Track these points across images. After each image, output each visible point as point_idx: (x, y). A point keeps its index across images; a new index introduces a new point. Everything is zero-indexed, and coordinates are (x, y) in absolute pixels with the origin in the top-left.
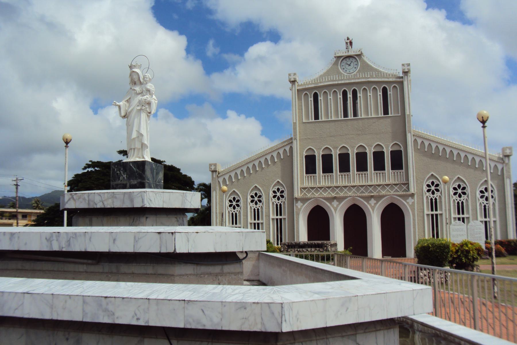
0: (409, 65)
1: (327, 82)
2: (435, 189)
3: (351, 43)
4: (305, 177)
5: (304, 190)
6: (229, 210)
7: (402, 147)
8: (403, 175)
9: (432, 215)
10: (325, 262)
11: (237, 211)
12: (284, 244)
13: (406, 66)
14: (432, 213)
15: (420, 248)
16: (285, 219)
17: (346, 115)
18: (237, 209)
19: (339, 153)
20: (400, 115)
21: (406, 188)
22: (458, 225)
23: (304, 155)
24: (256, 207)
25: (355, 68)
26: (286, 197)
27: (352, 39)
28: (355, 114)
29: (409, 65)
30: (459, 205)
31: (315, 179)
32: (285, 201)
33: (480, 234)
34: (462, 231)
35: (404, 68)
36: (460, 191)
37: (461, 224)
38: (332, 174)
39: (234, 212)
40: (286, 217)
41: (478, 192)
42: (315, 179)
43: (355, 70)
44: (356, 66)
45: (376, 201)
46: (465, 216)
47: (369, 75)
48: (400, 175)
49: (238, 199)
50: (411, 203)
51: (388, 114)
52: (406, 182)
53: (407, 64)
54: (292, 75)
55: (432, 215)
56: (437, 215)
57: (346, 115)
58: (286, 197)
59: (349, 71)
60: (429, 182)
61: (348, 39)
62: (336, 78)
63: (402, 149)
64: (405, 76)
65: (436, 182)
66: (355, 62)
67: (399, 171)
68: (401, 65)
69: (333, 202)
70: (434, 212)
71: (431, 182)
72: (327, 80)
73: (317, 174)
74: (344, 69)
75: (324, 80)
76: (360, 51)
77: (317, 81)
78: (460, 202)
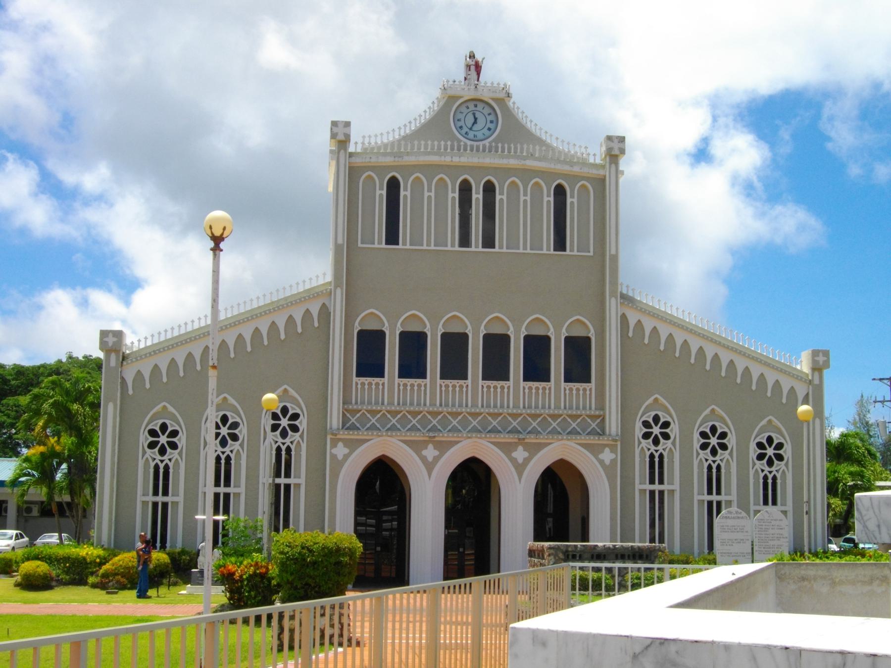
0: (347, 124)
1: (429, 154)
2: (714, 436)
3: (478, 68)
4: (482, 386)
5: (495, 419)
6: (147, 456)
7: (592, 331)
8: (590, 394)
9: (652, 493)
10: (601, 595)
11: (170, 460)
12: (557, 549)
13: (616, 141)
14: (652, 487)
15: (283, 566)
16: (672, 492)
17: (465, 241)
18: (778, 465)
19: (402, 330)
20: (591, 254)
21: (495, 426)
22: (734, 518)
23: (564, 334)
24: (223, 453)
25: (489, 129)
26: (142, 431)
27: (484, 59)
28: (489, 241)
29: (347, 124)
30: (712, 472)
31: (381, 390)
32: (301, 442)
33: (778, 539)
34: (742, 532)
35: (611, 145)
36: (714, 441)
37: (739, 516)
38: (547, 383)
39: (162, 461)
40: (302, 481)
41: (753, 446)
42: (547, 395)
43: (487, 133)
44: (492, 126)
45: (528, 452)
46: (722, 498)
47: (525, 152)
48: (544, 393)
49: (173, 428)
50: (607, 462)
51: (564, 250)
52: (597, 413)
53: (618, 137)
54: (341, 126)
55: (652, 493)
56: (661, 493)
57: (465, 241)
58: (142, 431)
59: (475, 136)
60: (649, 417)
61: (472, 56)
62: (419, 149)
63: (592, 335)
64: (610, 164)
65: (663, 416)
66: (489, 114)
67: (581, 386)
68: (348, 120)
69: (426, 450)
70: (657, 487)
71: (652, 417)
72: (512, 153)
73: (469, 381)
74: (461, 127)
75: (415, 150)
76: (504, 91)
77: (399, 148)
78: (714, 466)
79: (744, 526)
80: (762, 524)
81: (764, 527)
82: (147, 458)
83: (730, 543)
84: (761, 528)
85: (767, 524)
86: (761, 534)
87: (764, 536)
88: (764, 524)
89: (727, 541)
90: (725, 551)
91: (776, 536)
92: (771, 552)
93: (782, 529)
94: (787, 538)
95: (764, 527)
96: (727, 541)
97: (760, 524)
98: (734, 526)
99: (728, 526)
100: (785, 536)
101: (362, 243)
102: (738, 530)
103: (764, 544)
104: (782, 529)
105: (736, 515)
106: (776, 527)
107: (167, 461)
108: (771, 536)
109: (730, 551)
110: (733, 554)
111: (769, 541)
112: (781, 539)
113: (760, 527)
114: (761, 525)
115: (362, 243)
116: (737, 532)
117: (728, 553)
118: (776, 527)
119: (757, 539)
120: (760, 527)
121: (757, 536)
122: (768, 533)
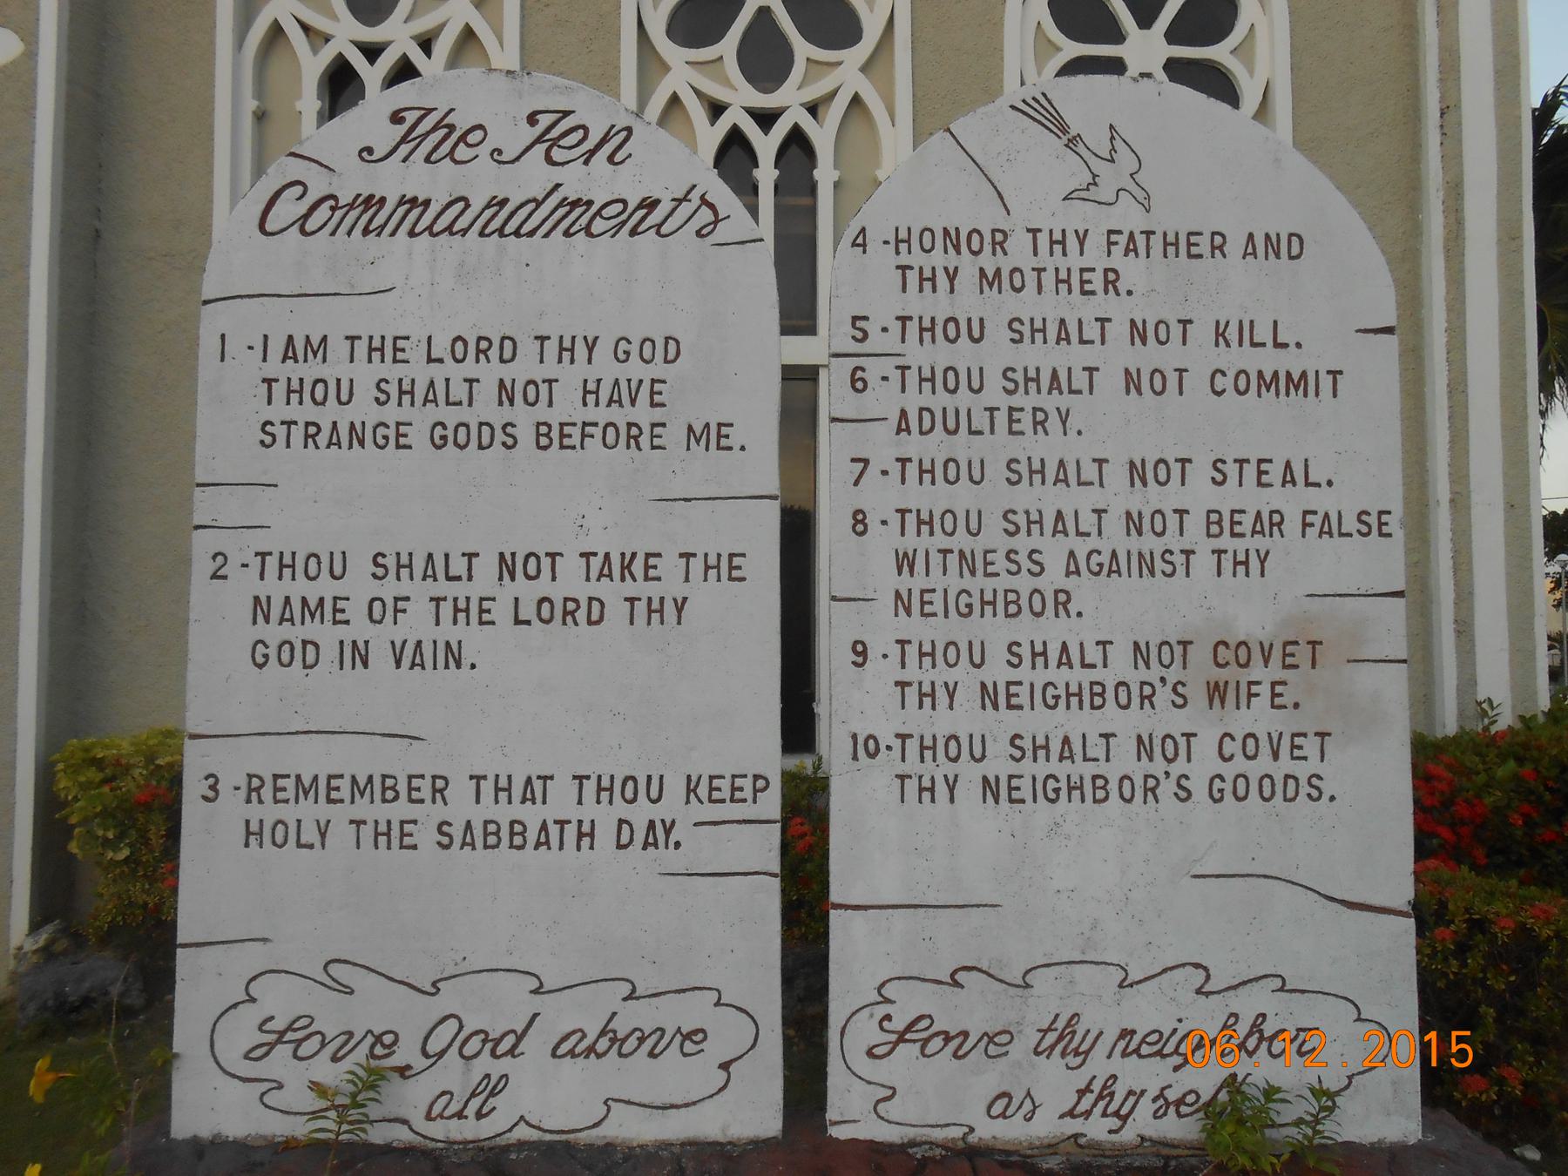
79: (672, 348)
80: (968, 302)
81: (997, 353)
82: (675, 100)
83: (417, 624)
84: (950, 378)
85: (1048, 306)
86: (951, 471)
87: (995, 496)
88: (999, 307)
89: (359, 586)
90: (311, 759)
91: (1199, 494)
92: (1125, 760)
93: (1297, 383)
94: (1372, 524)
95: (997, 353)
96: (359, 586)
97: (920, 304)
98: (508, 348)
99: (389, 348)
100: (1342, 501)
101: (1457, 1037)
102: (567, 406)
103: (995, 632)
104: (1297, 383)
105: (532, 177)
106: (1201, 355)
107: (796, 116)
108: (1119, 496)
109: (397, 761)
110: (461, 807)
111: (1084, 590)
112: (1288, 547)
113: (938, 355)
114: (951, 329)
115: (1457, 1037)
116: (544, 436)
117: (388, 789)
118: (1201, 355)
119: (883, 542)
120: (938, 355)
121: (881, 497)
122: (1048, 447)
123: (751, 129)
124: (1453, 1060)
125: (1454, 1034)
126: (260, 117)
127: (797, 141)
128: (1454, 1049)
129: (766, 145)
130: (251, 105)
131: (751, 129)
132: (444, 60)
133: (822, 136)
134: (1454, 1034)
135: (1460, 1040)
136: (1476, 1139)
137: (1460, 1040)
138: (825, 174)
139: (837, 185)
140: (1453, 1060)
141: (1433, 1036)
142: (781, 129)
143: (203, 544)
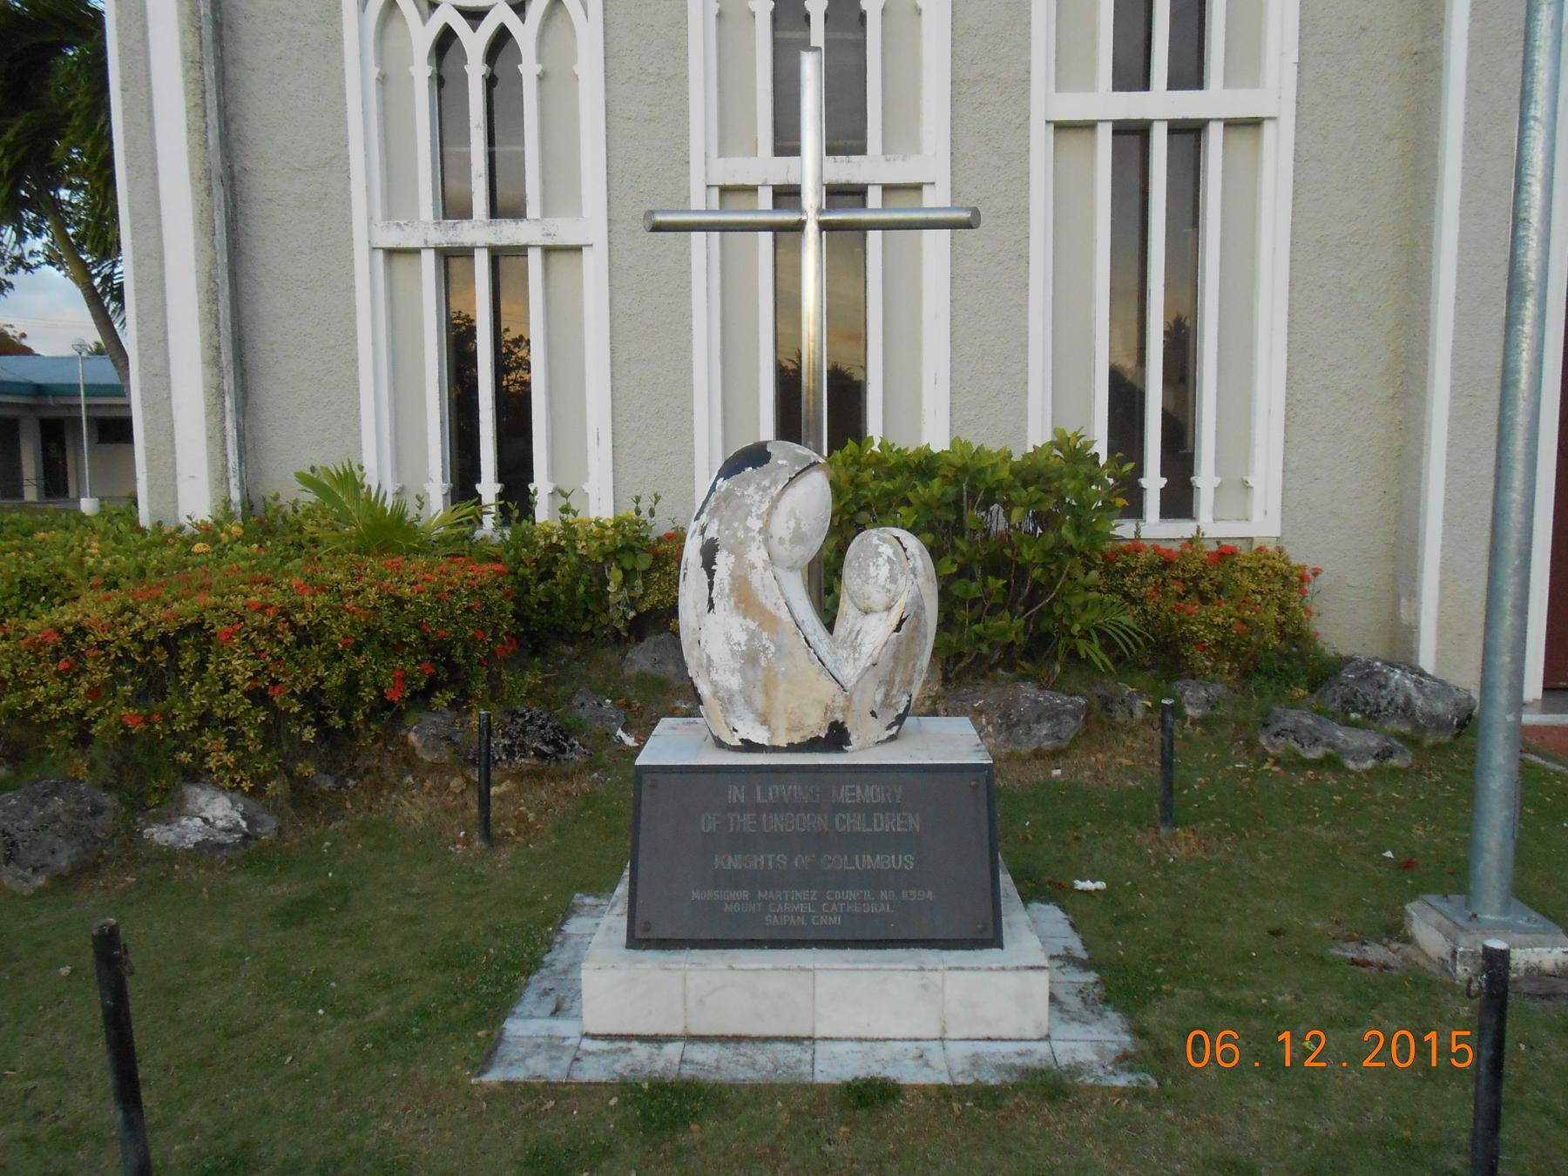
123: (460, 26)
124: (1453, 1060)
125: (1454, 1034)
126: (383, 79)
127: (502, 37)
128: (1454, 1049)
129: (474, 42)
130: (374, 72)
131: (460, 26)
132: (1178, 116)
133: (525, 34)
134: (1454, 1034)
135: (1459, 1040)
136: (1082, 947)
137: (1459, 1040)
138: (529, 69)
139: (541, 78)
140: (1453, 1060)
141: (1432, 1036)
142: (488, 27)
143: (848, 801)
